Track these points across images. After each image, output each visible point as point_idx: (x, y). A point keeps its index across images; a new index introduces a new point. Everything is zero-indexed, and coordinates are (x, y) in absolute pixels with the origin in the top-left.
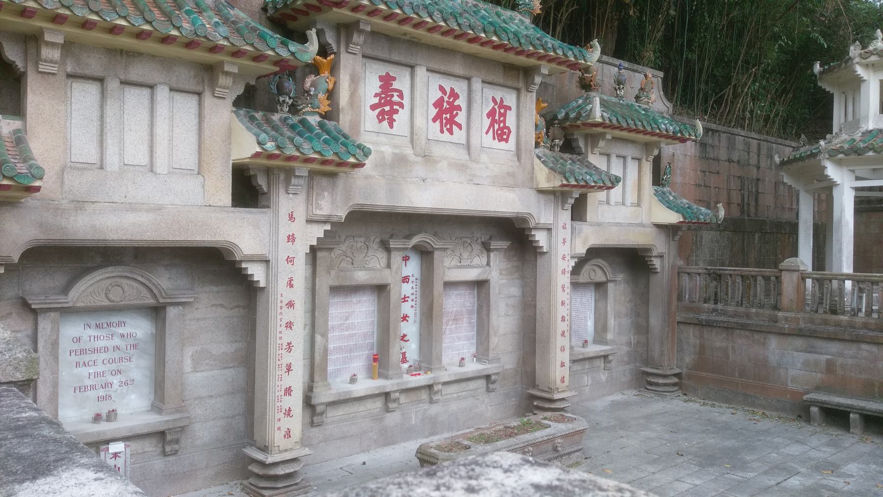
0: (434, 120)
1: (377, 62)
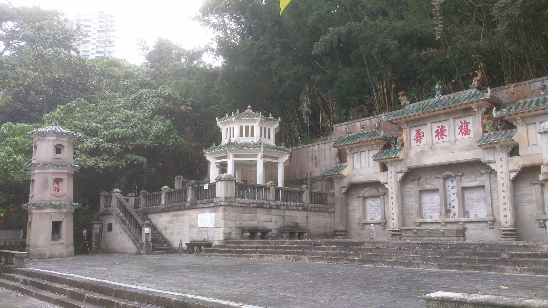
0: (436, 137)
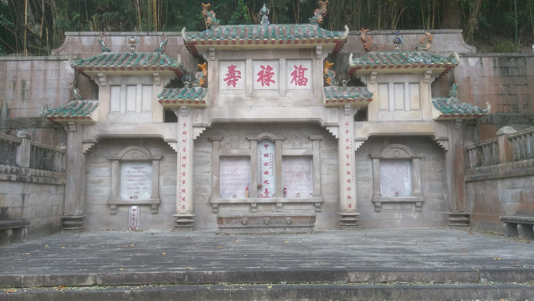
0: (258, 81)
1: (225, 61)
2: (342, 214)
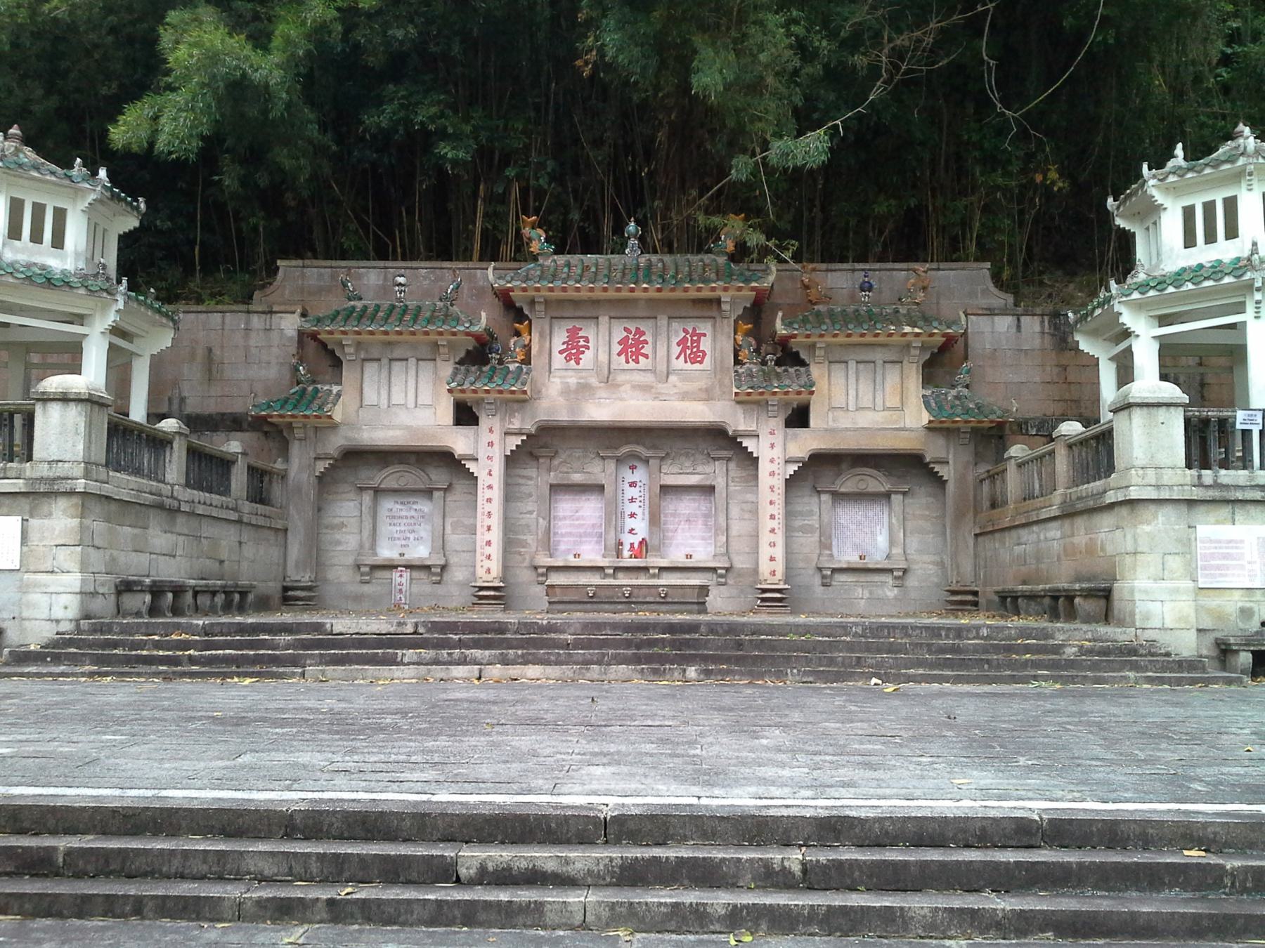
0: (619, 354)
2: (759, 586)
